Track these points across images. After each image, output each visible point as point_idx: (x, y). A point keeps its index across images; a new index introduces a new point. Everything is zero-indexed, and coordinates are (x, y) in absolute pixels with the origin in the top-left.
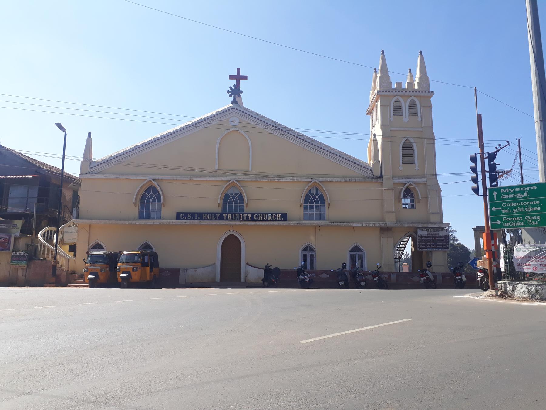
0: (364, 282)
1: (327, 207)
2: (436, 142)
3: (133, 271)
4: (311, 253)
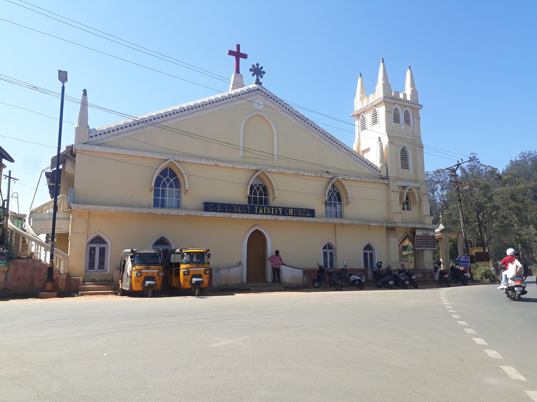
1: (345, 205)
2: (424, 150)
3: (205, 274)
4: (330, 251)
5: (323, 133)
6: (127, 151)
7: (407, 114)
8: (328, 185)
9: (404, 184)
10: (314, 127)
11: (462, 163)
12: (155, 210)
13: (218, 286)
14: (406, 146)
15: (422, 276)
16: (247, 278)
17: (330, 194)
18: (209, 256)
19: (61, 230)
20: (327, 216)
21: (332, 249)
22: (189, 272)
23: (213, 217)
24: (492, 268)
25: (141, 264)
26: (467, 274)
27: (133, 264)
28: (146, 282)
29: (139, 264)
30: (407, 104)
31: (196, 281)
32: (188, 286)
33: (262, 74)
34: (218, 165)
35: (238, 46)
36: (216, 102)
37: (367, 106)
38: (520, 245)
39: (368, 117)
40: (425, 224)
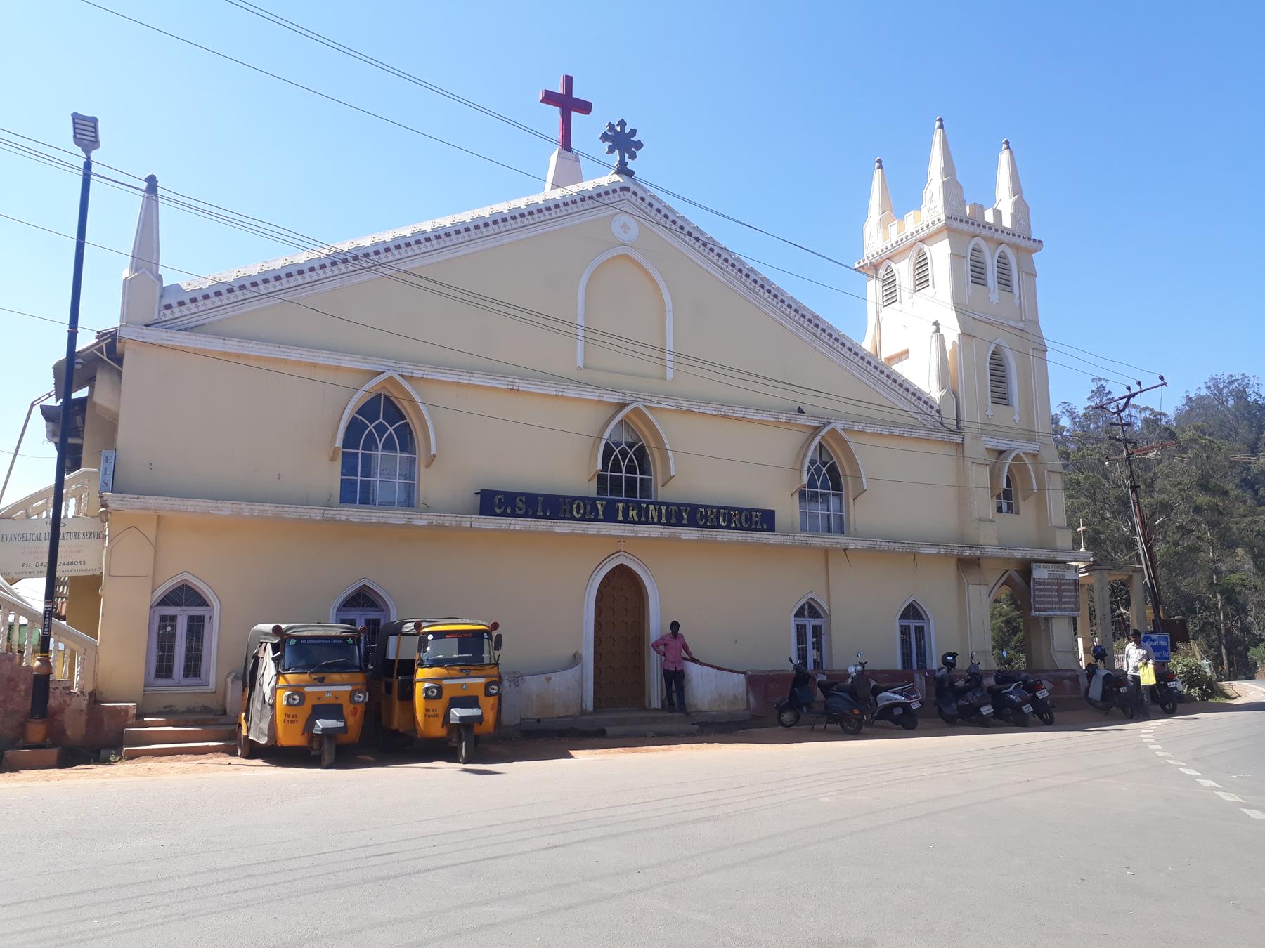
0: (1029, 705)
1: (851, 500)
2: (1049, 355)
3: (486, 695)
4: (813, 623)
5: (794, 306)
6: (269, 348)
7: (1003, 263)
8: (811, 441)
9: (1000, 444)
10: (769, 291)
11: (1140, 392)
12: (342, 512)
13: (518, 721)
14: (1004, 344)
15: (1052, 686)
16: (596, 699)
17: (812, 470)
18: (498, 642)
19: (82, 567)
20: (804, 529)
21: (819, 616)
22: (440, 689)
23: (503, 529)
24: (1202, 659)
25: (300, 669)
26: (1175, 683)
27: (280, 670)
28: (317, 721)
29: (297, 668)
30: (1004, 237)
31: (461, 718)
32: (437, 730)
33: (634, 149)
34: (518, 390)
35: (568, 81)
36: (514, 218)
37: (900, 242)
38: (1219, 597)
39: (903, 270)
40: (1056, 550)
